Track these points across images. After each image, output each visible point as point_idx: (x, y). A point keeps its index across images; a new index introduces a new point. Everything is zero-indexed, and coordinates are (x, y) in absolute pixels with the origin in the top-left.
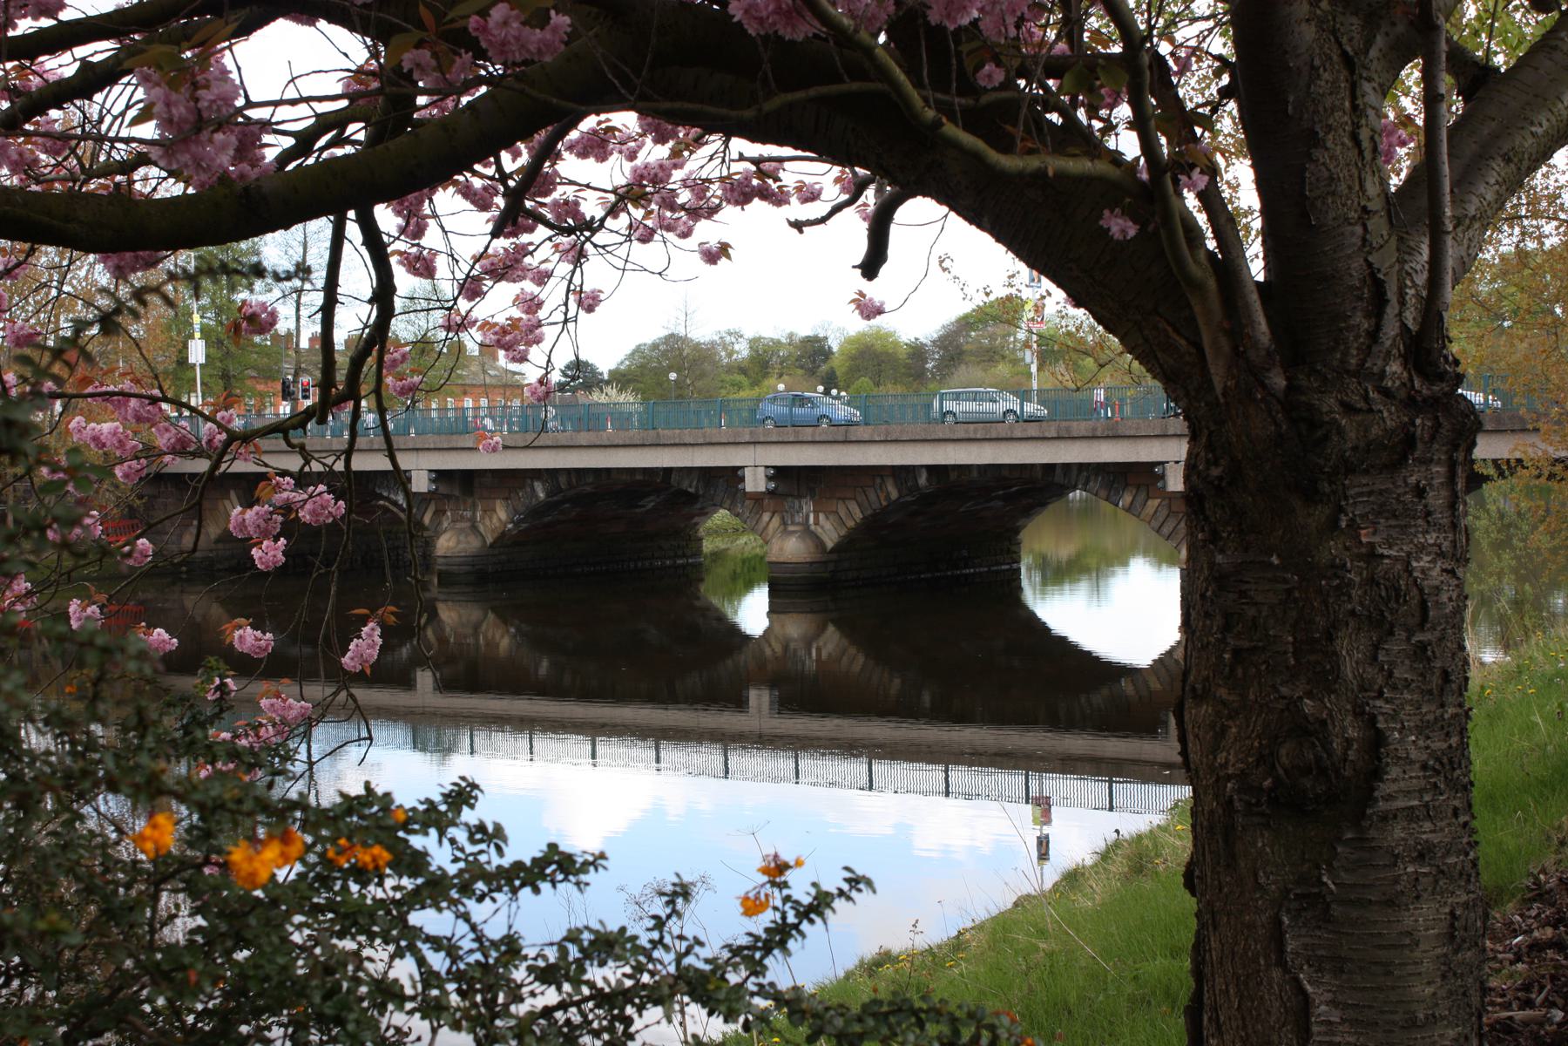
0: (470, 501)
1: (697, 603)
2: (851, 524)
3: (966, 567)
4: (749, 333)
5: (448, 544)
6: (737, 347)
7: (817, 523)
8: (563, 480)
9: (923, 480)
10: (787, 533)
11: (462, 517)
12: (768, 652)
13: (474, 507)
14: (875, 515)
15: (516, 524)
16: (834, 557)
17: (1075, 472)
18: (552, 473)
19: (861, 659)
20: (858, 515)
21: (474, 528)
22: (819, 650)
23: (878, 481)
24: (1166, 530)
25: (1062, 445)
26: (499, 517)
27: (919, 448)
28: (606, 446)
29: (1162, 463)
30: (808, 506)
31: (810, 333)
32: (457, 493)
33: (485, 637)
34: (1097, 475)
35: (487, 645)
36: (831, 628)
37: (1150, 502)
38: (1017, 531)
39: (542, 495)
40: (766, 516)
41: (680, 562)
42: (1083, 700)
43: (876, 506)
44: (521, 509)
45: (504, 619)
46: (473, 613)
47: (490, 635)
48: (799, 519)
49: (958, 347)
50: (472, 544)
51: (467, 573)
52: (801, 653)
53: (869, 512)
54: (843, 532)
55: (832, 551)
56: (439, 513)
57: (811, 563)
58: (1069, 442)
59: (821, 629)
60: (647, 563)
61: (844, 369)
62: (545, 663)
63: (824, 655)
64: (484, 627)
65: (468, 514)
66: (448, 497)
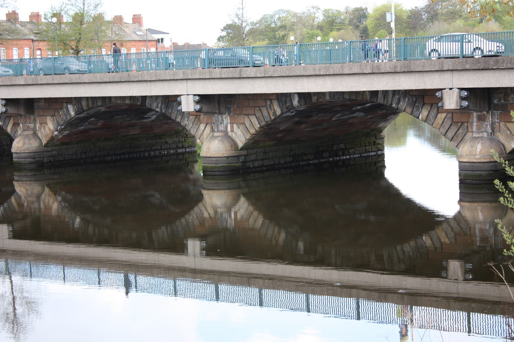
0: (32, 117)
1: (191, 177)
2: (253, 131)
3: (343, 155)
4: (323, 8)
5: (21, 145)
6: (317, 15)
7: (232, 131)
8: (84, 103)
9: (296, 102)
10: (214, 137)
11: (28, 127)
12: (206, 215)
13: (35, 121)
14: (267, 125)
15: (60, 131)
16: (244, 152)
17: (390, 96)
18: (78, 100)
19: (260, 220)
20: (257, 126)
21: (35, 134)
22: (236, 214)
23: (269, 103)
24: (450, 134)
25: (375, 78)
26: (48, 128)
27: (286, 81)
28: (100, 83)
29: (441, 90)
30: (226, 119)
31: (358, 7)
32: (22, 113)
33: (44, 202)
34: (405, 97)
35: (46, 207)
36: (243, 199)
37: (439, 115)
38: (380, 131)
39: (73, 114)
40: (202, 126)
41: (180, 151)
42: (398, 248)
43: (268, 119)
44: (62, 123)
45: (55, 192)
46: (36, 188)
47: (46, 201)
48: (222, 128)
49: (435, 11)
50: (33, 145)
51: (30, 163)
52: (225, 215)
53: (264, 123)
54: (248, 136)
55: (242, 149)
56: (16, 125)
57: (228, 157)
58: (381, 76)
59: (236, 200)
60: (157, 153)
61: (372, 25)
62: (78, 220)
63: (239, 217)
64: (43, 196)
65: (32, 125)
66: (21, 116)
